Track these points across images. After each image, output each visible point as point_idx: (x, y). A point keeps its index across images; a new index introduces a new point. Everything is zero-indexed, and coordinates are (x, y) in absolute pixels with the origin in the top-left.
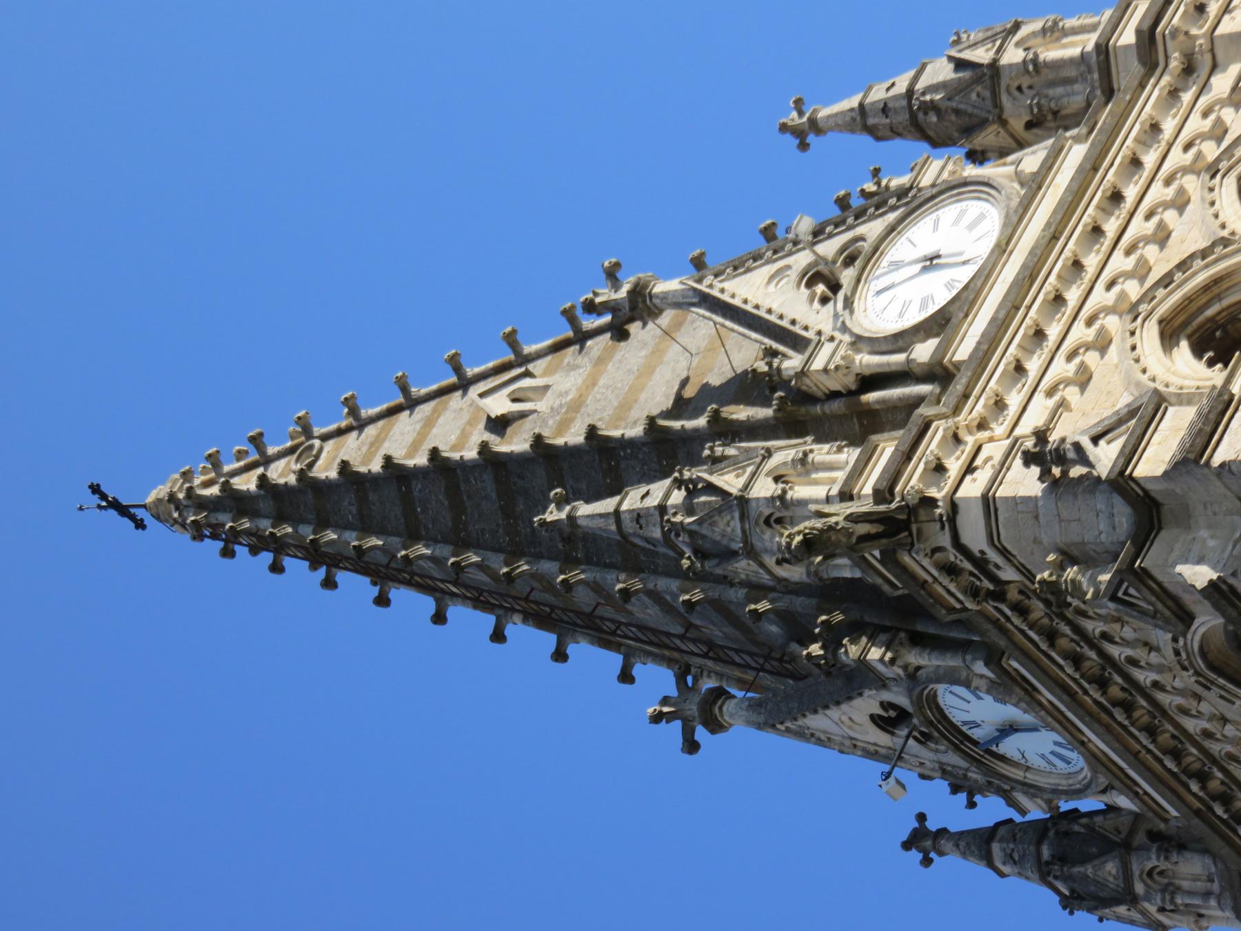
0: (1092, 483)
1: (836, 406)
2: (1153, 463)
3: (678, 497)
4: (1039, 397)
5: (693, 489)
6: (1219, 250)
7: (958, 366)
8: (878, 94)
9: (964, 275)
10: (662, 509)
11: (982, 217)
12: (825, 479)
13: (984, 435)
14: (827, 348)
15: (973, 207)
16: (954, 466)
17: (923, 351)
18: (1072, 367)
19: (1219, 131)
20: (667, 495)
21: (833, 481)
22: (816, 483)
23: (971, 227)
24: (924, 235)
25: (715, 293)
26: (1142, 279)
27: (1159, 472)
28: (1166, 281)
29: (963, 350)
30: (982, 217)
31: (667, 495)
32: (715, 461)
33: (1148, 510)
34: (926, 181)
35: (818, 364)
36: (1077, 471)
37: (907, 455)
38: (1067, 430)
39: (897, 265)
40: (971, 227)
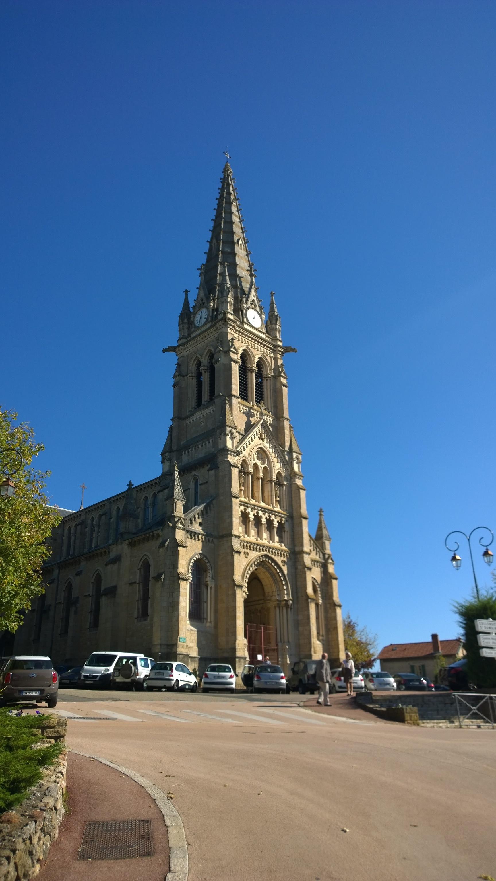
16: (231, 327)
17: (245, 320)
19: (267, 355)
29: (246, 326)
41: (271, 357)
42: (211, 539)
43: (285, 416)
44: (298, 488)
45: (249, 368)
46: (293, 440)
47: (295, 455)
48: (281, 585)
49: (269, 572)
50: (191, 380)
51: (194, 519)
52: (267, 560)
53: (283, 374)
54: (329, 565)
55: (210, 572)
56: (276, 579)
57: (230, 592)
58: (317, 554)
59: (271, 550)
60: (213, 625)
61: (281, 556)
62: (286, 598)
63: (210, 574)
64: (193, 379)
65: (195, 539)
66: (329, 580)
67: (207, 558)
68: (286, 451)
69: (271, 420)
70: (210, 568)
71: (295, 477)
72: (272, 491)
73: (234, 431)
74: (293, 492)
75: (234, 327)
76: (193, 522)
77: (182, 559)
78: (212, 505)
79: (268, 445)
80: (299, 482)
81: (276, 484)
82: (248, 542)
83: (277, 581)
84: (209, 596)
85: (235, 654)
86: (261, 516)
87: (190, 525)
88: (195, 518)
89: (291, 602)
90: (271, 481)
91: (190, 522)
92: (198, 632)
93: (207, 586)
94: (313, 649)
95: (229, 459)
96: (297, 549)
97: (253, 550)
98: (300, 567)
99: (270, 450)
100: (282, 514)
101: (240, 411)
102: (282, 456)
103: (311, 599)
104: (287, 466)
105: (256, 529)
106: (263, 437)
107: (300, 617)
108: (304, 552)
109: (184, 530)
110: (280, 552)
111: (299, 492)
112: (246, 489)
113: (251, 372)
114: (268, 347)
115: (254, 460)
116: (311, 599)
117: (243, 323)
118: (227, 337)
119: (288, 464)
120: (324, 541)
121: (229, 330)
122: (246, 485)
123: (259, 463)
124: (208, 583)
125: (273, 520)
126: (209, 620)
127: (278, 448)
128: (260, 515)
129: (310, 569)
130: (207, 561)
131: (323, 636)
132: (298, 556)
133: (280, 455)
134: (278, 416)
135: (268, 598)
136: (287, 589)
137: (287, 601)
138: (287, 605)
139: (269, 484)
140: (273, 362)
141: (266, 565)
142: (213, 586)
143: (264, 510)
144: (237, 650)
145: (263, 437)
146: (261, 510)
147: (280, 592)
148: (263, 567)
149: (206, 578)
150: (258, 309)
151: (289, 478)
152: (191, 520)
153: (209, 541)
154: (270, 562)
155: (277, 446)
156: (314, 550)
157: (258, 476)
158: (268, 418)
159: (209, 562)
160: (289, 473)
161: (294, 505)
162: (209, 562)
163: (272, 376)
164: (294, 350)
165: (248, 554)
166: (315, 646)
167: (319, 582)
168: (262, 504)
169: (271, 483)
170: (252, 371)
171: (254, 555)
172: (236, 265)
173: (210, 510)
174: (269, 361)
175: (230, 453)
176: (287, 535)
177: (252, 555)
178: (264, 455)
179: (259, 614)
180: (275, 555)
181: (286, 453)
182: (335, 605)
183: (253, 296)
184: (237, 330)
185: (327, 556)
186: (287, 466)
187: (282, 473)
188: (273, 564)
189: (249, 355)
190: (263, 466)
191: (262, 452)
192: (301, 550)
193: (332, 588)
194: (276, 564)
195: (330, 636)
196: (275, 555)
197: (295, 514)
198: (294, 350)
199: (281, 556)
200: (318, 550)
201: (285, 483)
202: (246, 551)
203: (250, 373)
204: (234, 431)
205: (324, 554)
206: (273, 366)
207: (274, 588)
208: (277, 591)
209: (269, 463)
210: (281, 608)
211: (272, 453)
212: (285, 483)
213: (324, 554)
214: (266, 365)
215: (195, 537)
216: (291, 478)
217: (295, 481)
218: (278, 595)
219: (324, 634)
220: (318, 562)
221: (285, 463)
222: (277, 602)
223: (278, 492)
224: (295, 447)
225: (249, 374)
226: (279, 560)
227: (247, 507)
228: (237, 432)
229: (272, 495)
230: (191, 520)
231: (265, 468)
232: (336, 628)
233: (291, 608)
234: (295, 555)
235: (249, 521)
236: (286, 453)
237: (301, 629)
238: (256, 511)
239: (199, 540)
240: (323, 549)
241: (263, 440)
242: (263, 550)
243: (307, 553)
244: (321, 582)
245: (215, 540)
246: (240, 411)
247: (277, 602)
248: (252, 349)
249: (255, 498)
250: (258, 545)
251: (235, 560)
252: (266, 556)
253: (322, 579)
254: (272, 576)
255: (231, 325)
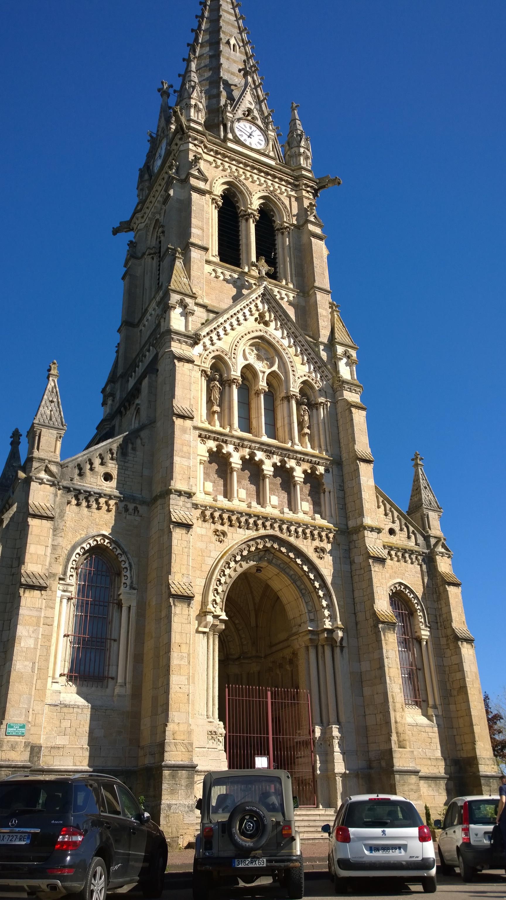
0: (307, 216)
1: (221, 119)
2: (193, 182)
3: (299, 132)
4: (213, 158)
5: (301, 136)
6: (249, 193)
7: (227, 144)
8: (298, 122)
9: (247, 143)
10: (297, 130)
11: (261, 144)
12: (198, 116)
13: (203, 147)
14: (231, 115)
15: (263, 143)
16: (196, 142)
17: (230, 136)
18: (277, 188)
19: (281, 193)
20: (300, 130)
21: (195, 117)
22: (194, 113)
23: (258, 143)
24: (257, 133)
25: (247, 89)
26: (245, 179)
27: (309, 228)
28: (280, 199)
29: (230, 145)
30: (261, 144)
31: (300, 130)
32: (307, 140)
33: (185, 181)
34: (269, 132)
35: (228, 114)
36: (309, 213)
37: (197, 131)
38: (202, 165)
39: (251, 128)
40: (258, 143)
41: (289, 197)
42: (131, 506)
43: (328, 298)
44: (350, 405)
45: (242, 213)
46: (338, 325)
47: (340, 350)
48: (315, 599)
49: (287, 574)
50: (150, 260)
51: (88, 466)
52: (276, 546)
53: (312, 219)
54: (438, 558)
55: (128, 574)
56: (306, 588)
57: (163, 614)
58: (409, 537)
59: (293, 528)
60: (128, 690)
61: (313, 539)
62: (328, 625)
63: (127, 577)
64: (153, 258)
65: (89, 507)
66: (441, 588)
67: (119, 546)
68: (322, 343)
69: (291, 295)
70: (127, 565)
71: (342, 388)
72: (290, 415)
73: (188, 300)
74: (339, 416)
75: (202, 142)
76: (88, 472)
77: (38, 543)
78: (139, 441)
79: (278, 334)
80: (352, 397)
81: (299, 404)
82: (222, 510)
83: (306, 592)
84: (123, 626)
85: (392, 766)
86: (261, 462)
87: (76, 477)
88: (91, 464)
89: (340, 634)
90: (288, 398)
91: (77, 471)
92: (92, 708)
93: (120, 605)
94: (394, 737)
95: (172, 349)
96: (351, 524)
97: (240, 527)
98: (359, 559)
99: (285, 342)
100: (313, 456)
101: (217, 277)
102: (310, 351)
103: (383, 623)
104: (323, 369)
105: (253, 488)
106: (267, 318)
107: (365, 666)
108: (365, 528)
109: (53, 485)
110: (309, 531)
111: (351, 412)
112: (226, 411)
113: (247, 220)
114: (281, 179)
115: (246, 359)
116: (383, 623)
117: (225, 140)
118: (188, 158)
119: (327, 368)
120: (425, 511)
121: (191, 146)
122: (226, 404)
123: (260, 366)
124: (121, 597)
125: (292, 469)
126: (120, 680)
127: (300, 338)
128: (257, 459)
129: (381, 561)
130: (119, 551)
131: (435, 707)
132: (355, 537)
133: (310, 352)
134: (305, 288)
135: (294, 630)
136: (330, 607)
137: (331, 632)
138: (331, 640)
139: (285, 403)
140: (295, 204)
141: (278, 558)
142: (134, 604)
143: (269, 451)
144: (167, 748)
145: (267, 318)
146: (259, 449)
147: (316, 616)
148: (270, 562)
149: (119, 588)
150: (259, 122)
151: (330, 391)
152: (80, 467)
153: (126, 510)
154: (284, 550)
155: (298, 334)
156: (401, 530)
157: (256, 388)
158: (283, 293)
159: (124, 552)
160: (330, 382)
161: (342, 441)
162: (124, 552)
163: (293, 225)
164: (335, 181)
165: (224, 534)
166: (400, 730)
167: (420, 595)
168: (265, 439)
169: (289, 401)
170: (247, 216)
171: (238, 536)
172: (220, 65)
173: (134, 449)
174: (287, 203)
175: (175, 337)
176: (329, 501)
177: (235, 535)
178: (271, 350)
179: (288, 668)
180: (297, 537)
181: (322, 347)
182: (457, 639)
183: (248, 101)
184: (212, 150)
185: (433, 541)
186: (323, 369)
187: (313, 382)
188: (292, 555)
189: (241, 192)
190: (268, 371)
191: (265, 346)
192: (359, 523)
193: (448, 604)
194: (299, 553)
195: (452, 707)
196: (297, 537)
197: (344, 456)
198: (335, 181)
199: (313, 539)
200: (411, 529)
201: (322, 400)
202: (220, 528)
203: (244, 221)
204: (188, 300)
205: (427, 538)
206: (295, 211)
207: (304, 608)
208: (310, 612)
209: (283, 365)
210: (320, 648)
211: (290, 347)
212: (322, 400)
213: (427, 538)
214: (279, 210)
215: (88, 501)
216: (334, 391)
217: (343, 396)
218: (311, 620)
219: (438, 702)
220: (412, 552)
221: (319, 364)
222: (310, 636)
223: (306, 418)
224: (341, 335)
225: (243, 224)
226: (307, 547)
227: (226, 442)
228: (197, 304)
229: (290, 424)
230: (80, 467)
231: (273, 374)
232: (463, 689)
233: (342, 648)
234: (348, 537)
235: (232, 470)
236: (322, 347)
237: (367, 691)
238: (248, 450)
239: (109, 511)
240: (424, 529)
241: (266, 324)
242: (264, 526)
243: (372, 529)
244: (424, 594)
245: (142, 509)
246: (217, 277)
247: (310, 636)
248: (248, 183)
249: (253, 431)
250: (249, 515)
251: (175, 542)
252: (273, 538)
253: (427, 588)
254: (294, 582)
255: (196, 139)
